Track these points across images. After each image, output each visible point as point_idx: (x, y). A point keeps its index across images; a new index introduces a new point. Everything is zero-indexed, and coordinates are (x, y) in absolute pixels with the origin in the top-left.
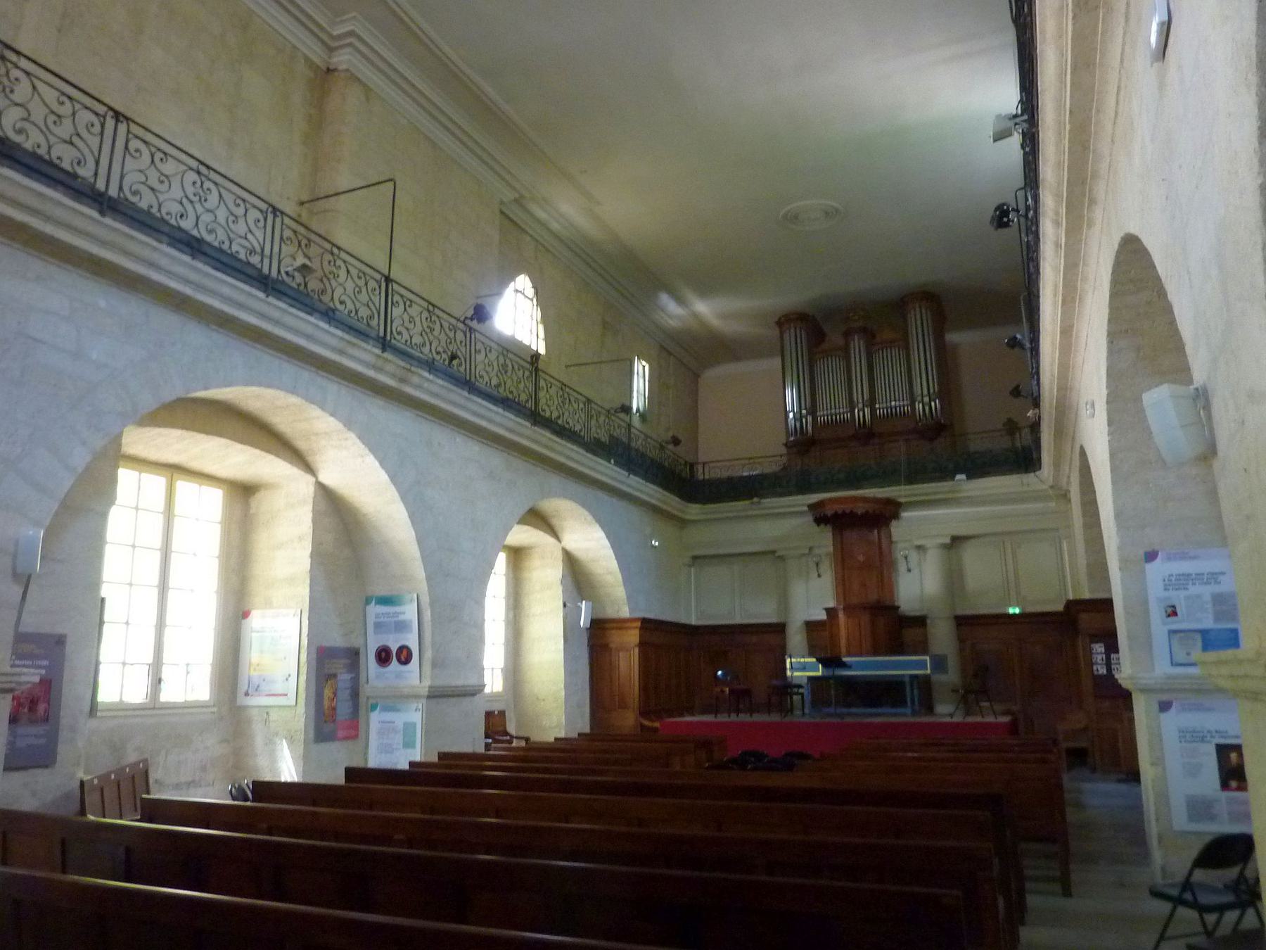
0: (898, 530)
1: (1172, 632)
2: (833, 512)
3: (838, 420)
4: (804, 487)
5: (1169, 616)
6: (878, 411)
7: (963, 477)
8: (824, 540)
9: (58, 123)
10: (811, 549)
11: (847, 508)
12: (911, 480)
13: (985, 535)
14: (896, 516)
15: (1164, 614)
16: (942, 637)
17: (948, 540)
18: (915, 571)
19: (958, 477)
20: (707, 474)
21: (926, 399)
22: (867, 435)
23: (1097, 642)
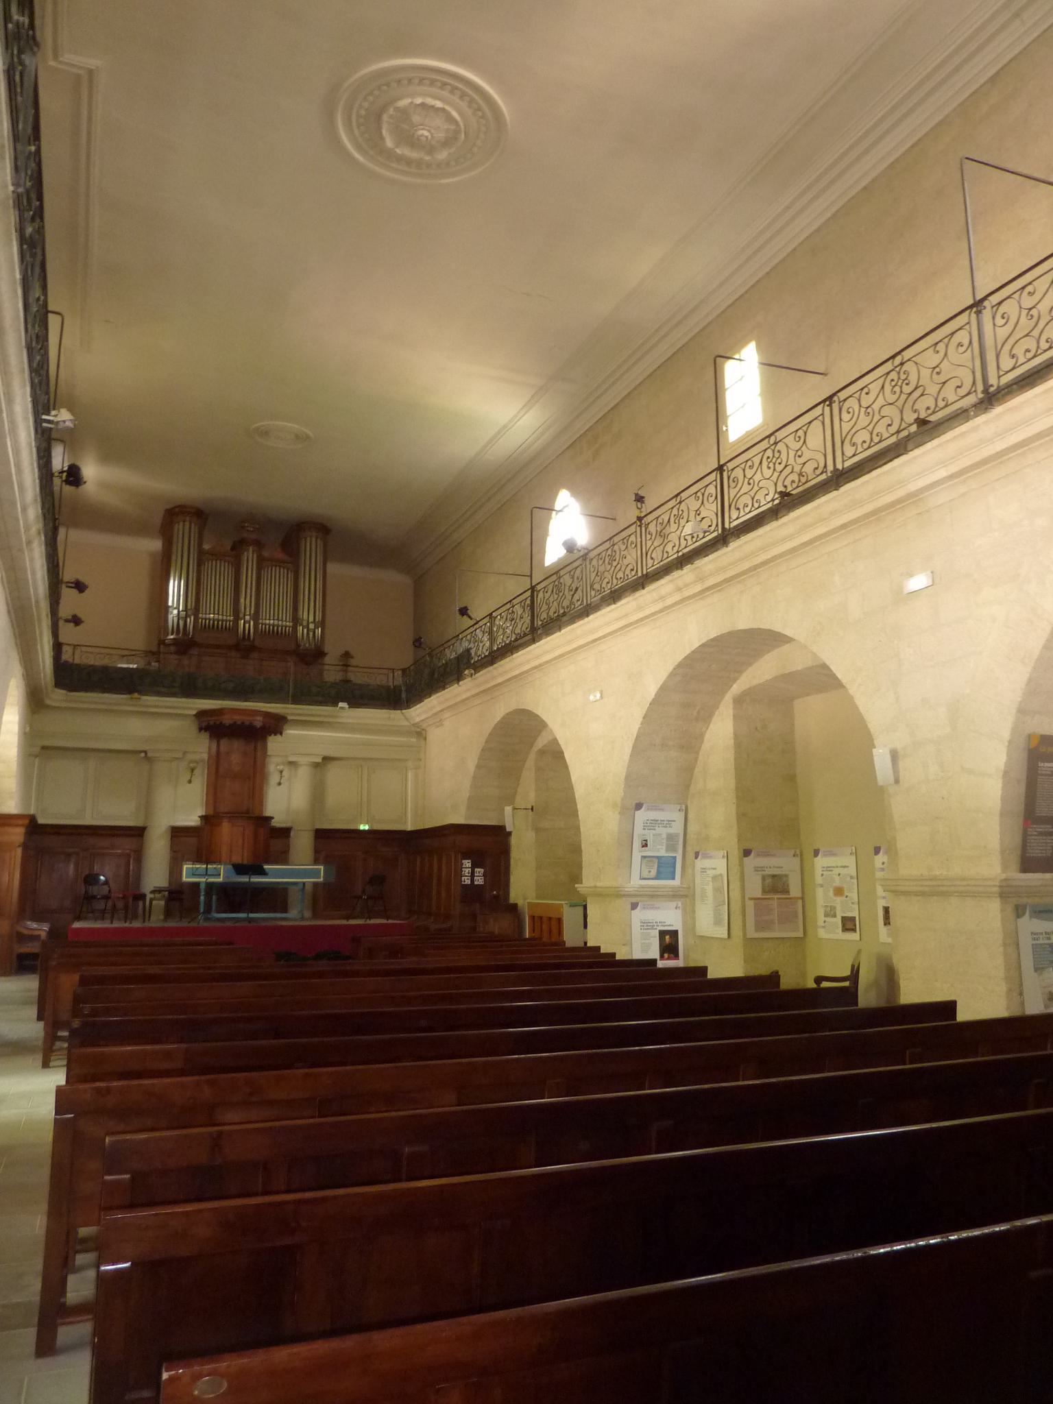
0: (274, 744)
1: (644, 857)
2: (231, 722)
3: (220, 627)
4: (189, 688)
5: (643, 847)
6: (200, 620)
7: (344, 705)
8: (202, 747)
9: (961, 349)
10: (185, 753)
11: (247, 720)
12: (296, 701)
13: (347, 759)
14: (278, 731)
15: (641, 846)
16: (302, 844)
17: (319, 760)
18: (284, 787)
19: (341, 704)
20: (77, 656)
21: (312, 626)
22: (244, 647)
23: (467, 859)
